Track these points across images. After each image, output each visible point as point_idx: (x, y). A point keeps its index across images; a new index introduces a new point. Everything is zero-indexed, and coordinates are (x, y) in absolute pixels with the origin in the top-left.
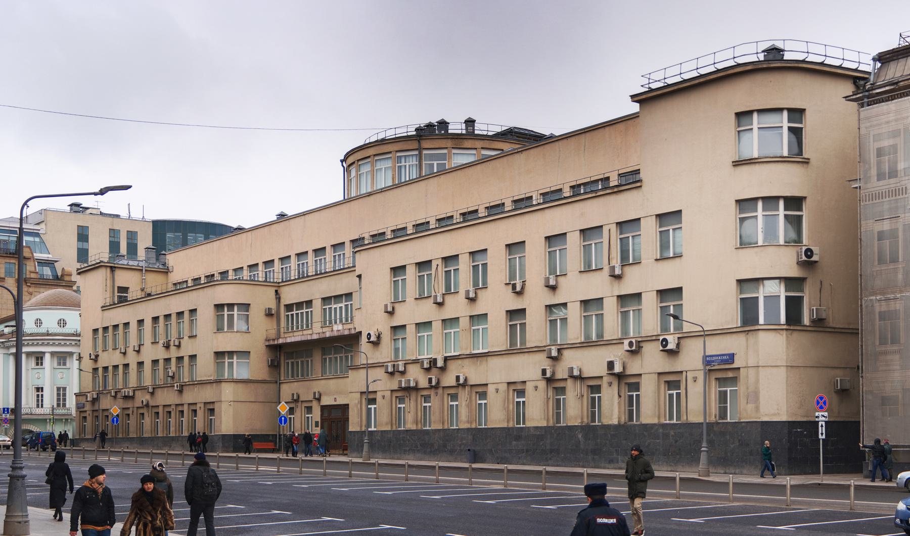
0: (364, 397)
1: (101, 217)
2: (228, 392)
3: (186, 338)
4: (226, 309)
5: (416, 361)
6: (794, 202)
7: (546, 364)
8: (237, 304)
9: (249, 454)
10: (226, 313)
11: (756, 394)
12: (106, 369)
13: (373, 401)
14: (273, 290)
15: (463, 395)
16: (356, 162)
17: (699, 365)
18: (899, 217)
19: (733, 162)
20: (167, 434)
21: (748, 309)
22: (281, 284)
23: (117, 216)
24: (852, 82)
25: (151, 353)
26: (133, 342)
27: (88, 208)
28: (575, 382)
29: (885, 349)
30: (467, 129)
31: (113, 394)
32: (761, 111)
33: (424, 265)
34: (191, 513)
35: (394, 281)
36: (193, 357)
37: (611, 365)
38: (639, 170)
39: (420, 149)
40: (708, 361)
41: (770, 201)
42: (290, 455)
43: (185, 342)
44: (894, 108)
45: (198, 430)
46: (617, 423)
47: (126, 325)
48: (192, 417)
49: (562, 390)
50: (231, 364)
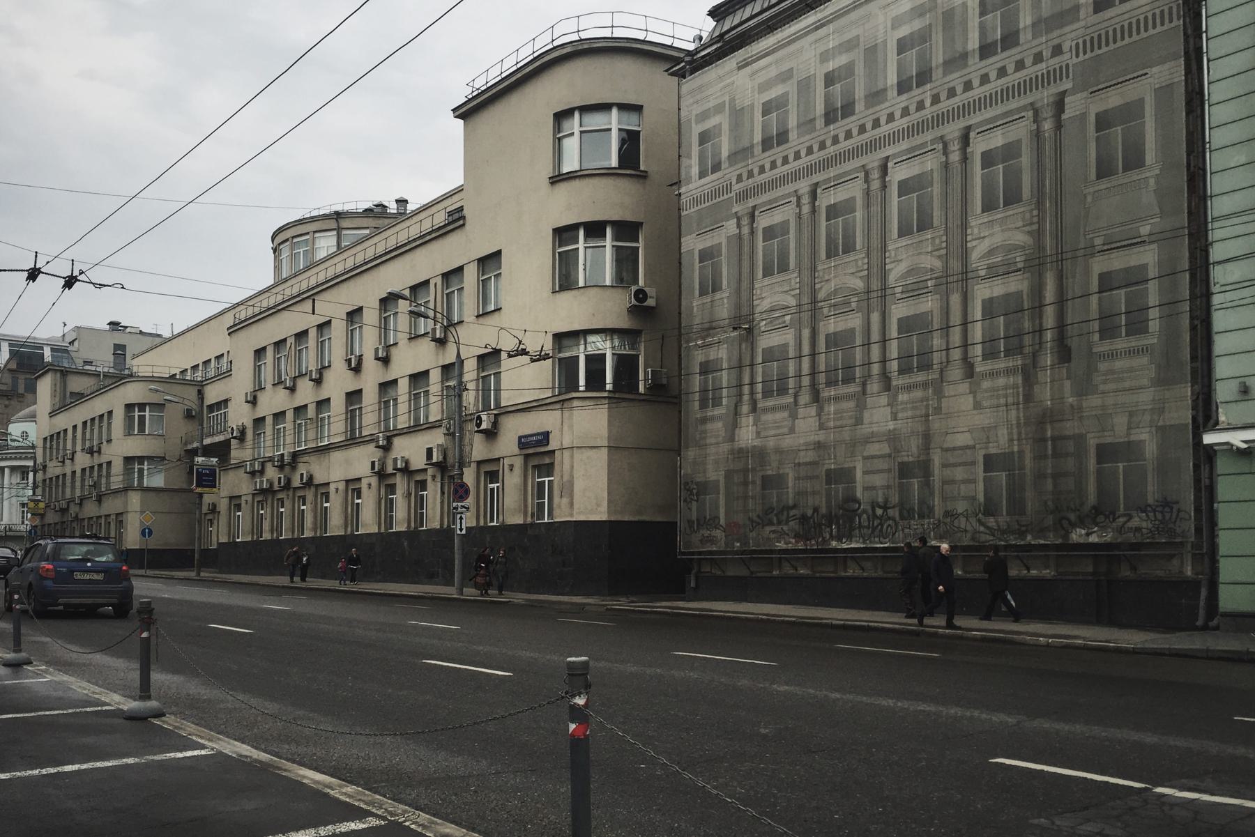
0: (827, 393)
1: (139, 336)
2: (135, 500)
3: (105, 443)
4: (136, 409)
5: (271, 459)
6: (627, 230)
7: (376, 455)
8: (149, 404)
9: (500, 593)
10: (137, 414)
11: (571, 483)
12: (51, 479)
13: (238, 507)
14: (196, 389)
15: (310, 495)
16: (290, 239)
17: (516, 450)
18: (1146, 74)
19: (550, 178)
20: (486, 522)
21: (567, 369)
22: (204, 383)
23: (159, 336)
24: (691, 454)
25: (82, 460)
26: (311, 363)
27: (127, 327)
28: (437, 355)
29: (1125, 346)
30: (398, 209)
31: (77, 501)
32: (586, 109)
33: (279, 344)
34: (873, 610)
35: (483, 377)
36: (109, 463)
37: (429, 451)
38: (461, 209)
39: (339, 230)
40: (523, 442)
41: (595, 230)
42: (297, 579)
43: (104, 447)
44: (929, 236)
45: (436, 486)
46: (439, 527)
47: (65, 431)
48: (386, 495)
49: (391, 489)
50: (141, 471)
